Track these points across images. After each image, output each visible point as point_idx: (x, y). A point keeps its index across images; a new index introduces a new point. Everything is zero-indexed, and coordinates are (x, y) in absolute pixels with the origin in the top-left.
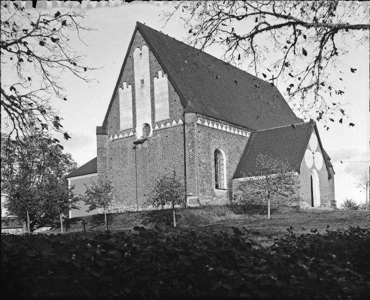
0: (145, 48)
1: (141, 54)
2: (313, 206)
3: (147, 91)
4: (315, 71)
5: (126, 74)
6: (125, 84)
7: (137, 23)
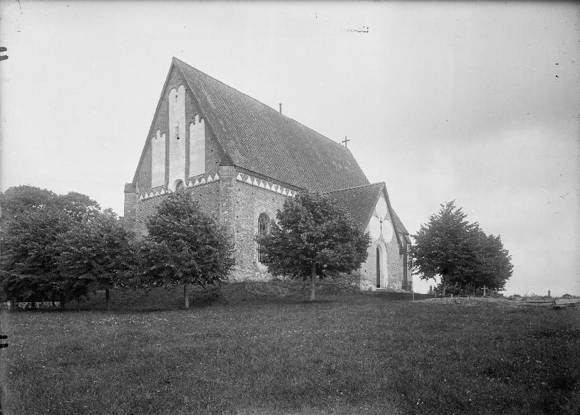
0: (182, 89)
1: (177, 96)
2: (378, 286)
3: (182, 141)
4: (180, 126)
5: (160, 123)
6: (158, 133)
7: (174, 58)
